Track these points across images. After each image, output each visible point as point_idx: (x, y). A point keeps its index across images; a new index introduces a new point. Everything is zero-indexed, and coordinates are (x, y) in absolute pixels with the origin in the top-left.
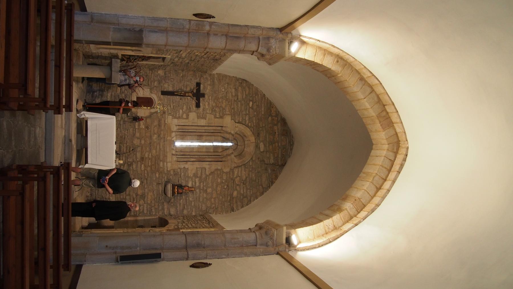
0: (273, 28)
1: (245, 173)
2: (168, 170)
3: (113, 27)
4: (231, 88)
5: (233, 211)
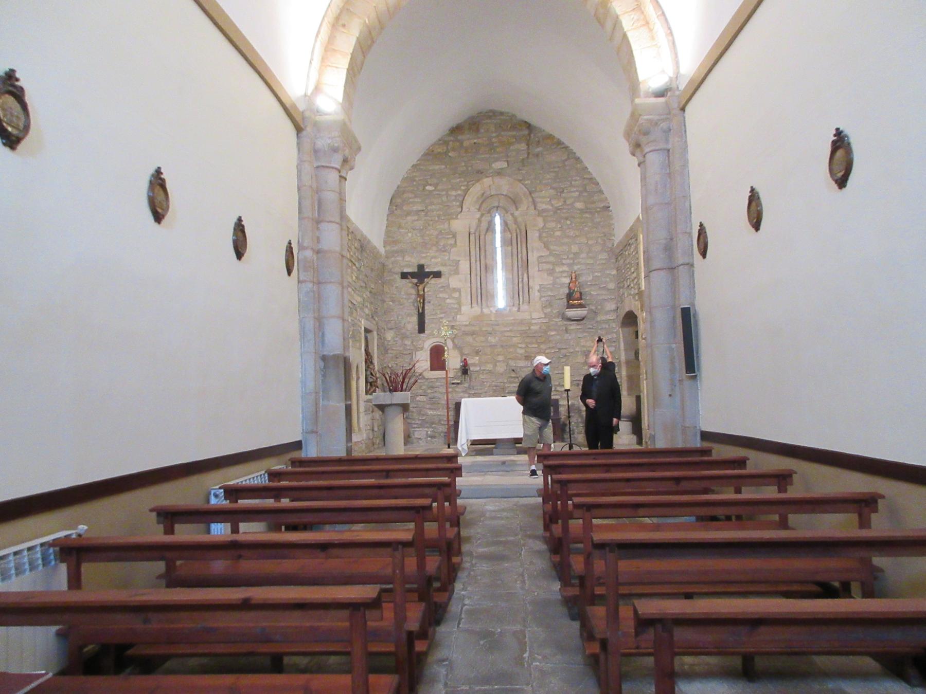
0: (298, 144)
1: (543, 192)
2: (543, 316)
3: (321, 400)
4: (407, 223)
5: (609, 207)
